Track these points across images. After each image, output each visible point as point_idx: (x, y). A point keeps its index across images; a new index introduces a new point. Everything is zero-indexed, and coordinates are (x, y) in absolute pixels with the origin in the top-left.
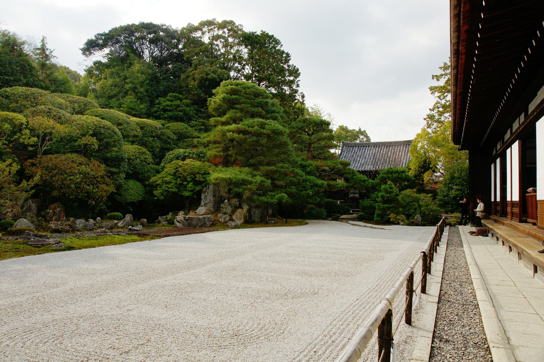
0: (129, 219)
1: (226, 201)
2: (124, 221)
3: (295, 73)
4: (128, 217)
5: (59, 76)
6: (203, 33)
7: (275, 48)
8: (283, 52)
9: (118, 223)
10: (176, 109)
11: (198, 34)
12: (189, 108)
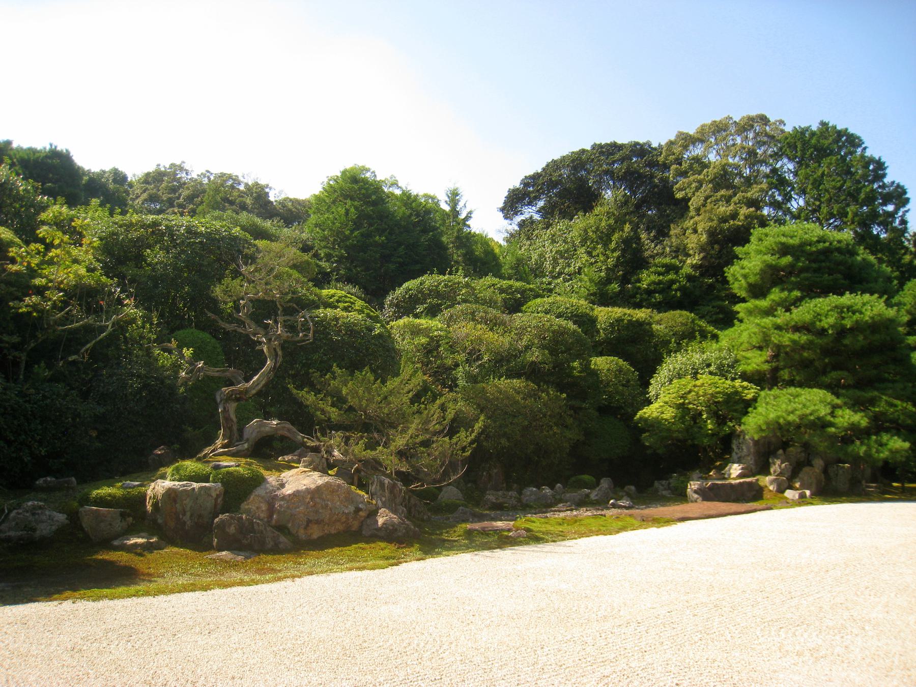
2: (223, 371)
3: (899, 196)
4: (605, 483)
5: (501, 258)
8: (871, 160)
11: (697, 151)
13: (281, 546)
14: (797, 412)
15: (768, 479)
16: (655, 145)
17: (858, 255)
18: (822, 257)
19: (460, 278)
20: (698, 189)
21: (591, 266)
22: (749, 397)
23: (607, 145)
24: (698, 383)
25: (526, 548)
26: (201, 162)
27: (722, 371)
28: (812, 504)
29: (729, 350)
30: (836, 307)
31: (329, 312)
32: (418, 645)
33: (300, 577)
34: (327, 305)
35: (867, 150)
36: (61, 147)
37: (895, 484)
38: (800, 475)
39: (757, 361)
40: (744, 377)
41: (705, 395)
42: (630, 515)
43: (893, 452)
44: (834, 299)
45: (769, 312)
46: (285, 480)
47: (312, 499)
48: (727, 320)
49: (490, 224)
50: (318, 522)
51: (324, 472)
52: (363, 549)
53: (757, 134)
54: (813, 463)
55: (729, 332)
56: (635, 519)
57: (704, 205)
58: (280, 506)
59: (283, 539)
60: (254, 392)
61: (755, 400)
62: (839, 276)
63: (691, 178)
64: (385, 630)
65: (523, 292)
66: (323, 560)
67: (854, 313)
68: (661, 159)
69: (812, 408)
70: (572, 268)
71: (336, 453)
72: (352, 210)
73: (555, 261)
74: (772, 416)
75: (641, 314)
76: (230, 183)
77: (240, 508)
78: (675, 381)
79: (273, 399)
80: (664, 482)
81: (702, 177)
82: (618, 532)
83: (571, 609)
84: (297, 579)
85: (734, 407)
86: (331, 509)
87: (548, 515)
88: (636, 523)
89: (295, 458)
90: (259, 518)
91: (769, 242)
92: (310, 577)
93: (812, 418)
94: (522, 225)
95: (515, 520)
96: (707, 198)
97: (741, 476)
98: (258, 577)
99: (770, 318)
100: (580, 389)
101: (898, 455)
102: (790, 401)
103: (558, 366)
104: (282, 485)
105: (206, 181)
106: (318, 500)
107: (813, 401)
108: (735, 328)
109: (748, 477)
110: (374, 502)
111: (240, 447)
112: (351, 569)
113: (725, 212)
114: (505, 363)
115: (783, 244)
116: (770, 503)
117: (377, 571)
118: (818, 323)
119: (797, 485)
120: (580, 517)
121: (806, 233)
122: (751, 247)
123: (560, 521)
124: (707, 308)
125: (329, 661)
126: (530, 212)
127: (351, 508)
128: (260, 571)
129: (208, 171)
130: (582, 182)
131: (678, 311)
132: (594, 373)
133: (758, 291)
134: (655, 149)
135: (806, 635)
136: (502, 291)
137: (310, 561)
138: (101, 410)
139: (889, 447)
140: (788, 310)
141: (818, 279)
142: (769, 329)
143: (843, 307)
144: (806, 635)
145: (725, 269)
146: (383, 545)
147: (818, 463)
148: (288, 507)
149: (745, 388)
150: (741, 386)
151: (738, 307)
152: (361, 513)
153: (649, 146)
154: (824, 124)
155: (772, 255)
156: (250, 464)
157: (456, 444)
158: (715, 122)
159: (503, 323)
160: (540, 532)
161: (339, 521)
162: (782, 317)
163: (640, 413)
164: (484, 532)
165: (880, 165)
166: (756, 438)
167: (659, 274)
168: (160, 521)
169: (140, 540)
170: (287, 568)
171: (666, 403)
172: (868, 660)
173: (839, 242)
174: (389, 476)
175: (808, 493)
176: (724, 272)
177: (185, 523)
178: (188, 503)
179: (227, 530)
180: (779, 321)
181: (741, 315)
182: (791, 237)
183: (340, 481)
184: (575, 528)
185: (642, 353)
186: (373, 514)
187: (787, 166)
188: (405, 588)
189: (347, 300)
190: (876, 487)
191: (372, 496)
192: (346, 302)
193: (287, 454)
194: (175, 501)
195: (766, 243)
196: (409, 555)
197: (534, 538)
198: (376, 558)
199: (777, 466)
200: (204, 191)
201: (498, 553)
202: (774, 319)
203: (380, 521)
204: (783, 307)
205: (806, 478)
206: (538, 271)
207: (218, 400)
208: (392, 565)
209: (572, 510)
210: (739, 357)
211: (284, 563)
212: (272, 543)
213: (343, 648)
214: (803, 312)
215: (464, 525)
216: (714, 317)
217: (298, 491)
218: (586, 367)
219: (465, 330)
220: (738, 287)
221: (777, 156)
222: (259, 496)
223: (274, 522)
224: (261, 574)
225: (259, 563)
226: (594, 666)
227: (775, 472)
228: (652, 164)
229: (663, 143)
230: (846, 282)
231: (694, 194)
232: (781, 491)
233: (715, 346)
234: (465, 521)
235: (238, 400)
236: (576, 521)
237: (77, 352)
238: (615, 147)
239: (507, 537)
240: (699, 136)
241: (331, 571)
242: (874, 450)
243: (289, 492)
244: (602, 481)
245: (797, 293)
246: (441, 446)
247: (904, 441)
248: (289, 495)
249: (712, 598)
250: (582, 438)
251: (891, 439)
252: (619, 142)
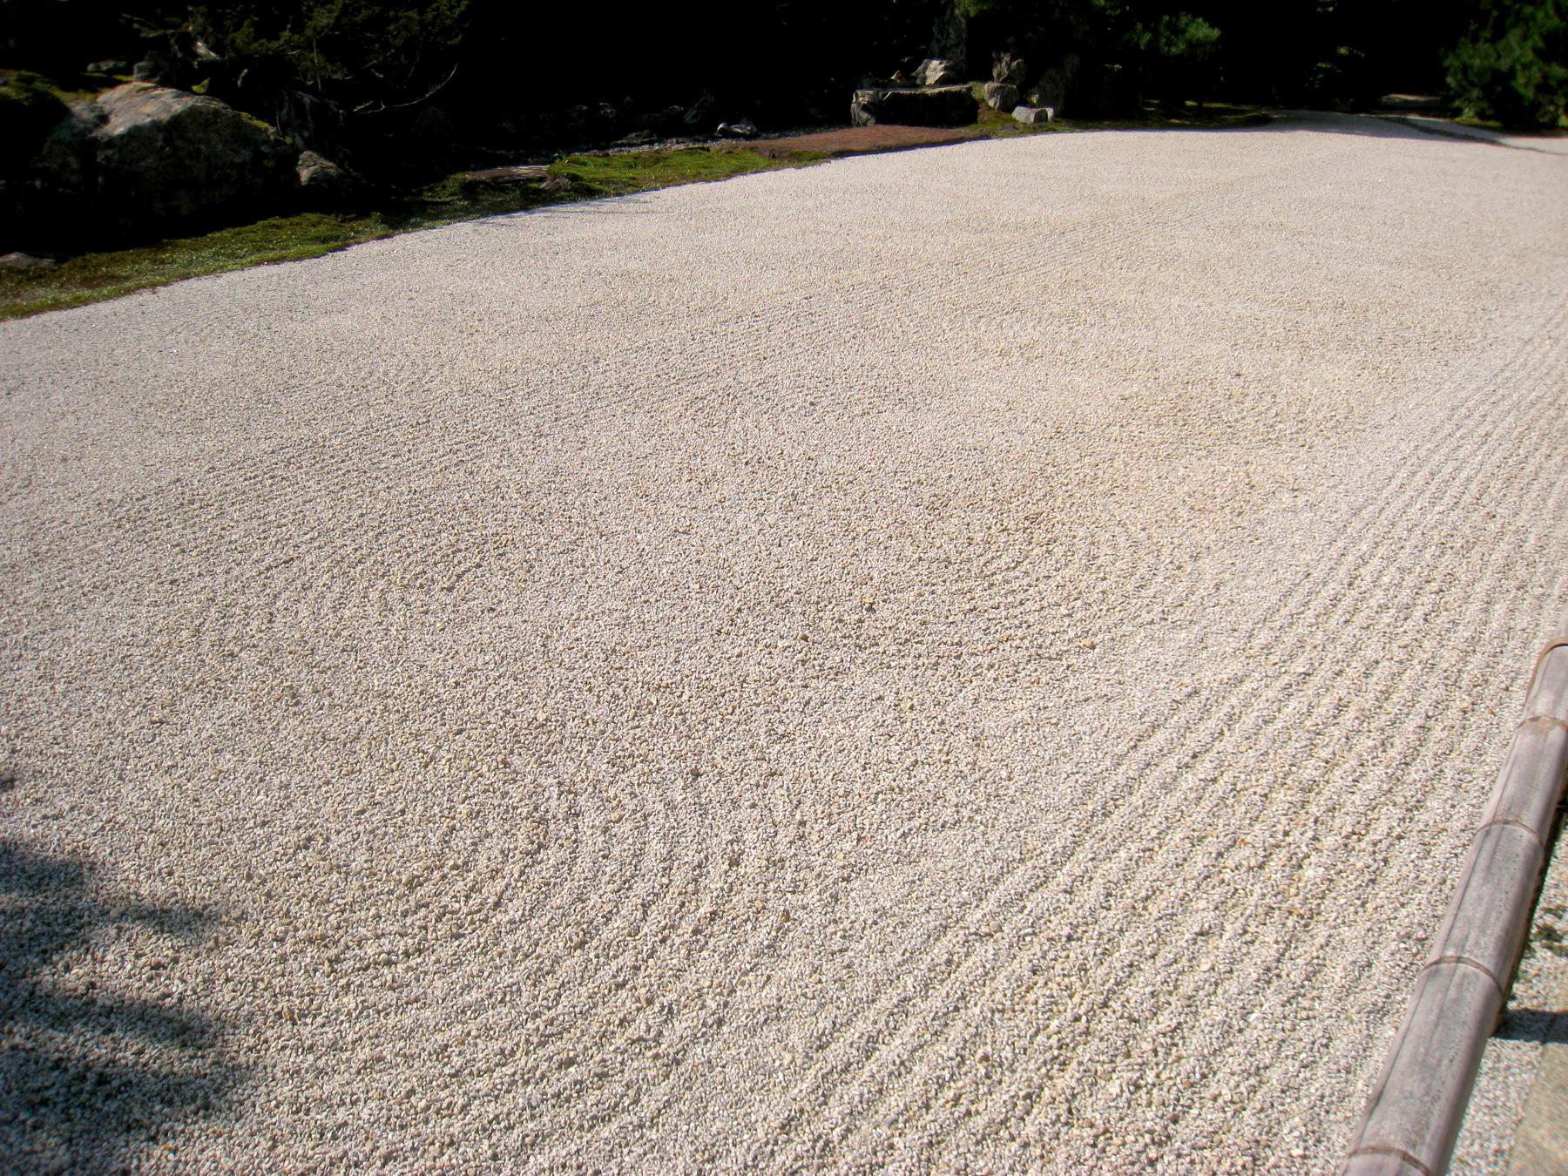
15: (987, 86)
25: (570, 208)
28: (1055, 131)
32: (386, 374)
33: (166, 284)
37: (1189, 103)
42: (752, 149)
43: (1193, 45)
46: (107, 108)
51: (184, 87)
52: (278, 227)
58: (107, 158)
64: (328, 355)
66: (206, 253)
71: (201, 48)
82: (729, 176)
83: (645, 300)
84: (162, 289)
87: (610, 152)
88: (762, 161)
89: (122, 64)
92: (185, 283)
95: (552, 162)
97: (942, 81)
98: (87, 293)
101: (1199, 51)
104: (104, 119)
106: (179, 143)
109: (955, 83)
110: (288, 140)
112: (258, 264)
116: (986, 129)
117: (306, 263)
119: (1034, 99)
120: (665, 154)
123: (631, 161)
125: (233, 413)
128: (88, 282)
135: (1017, 327)
137: (182, 257)
139: (1187, 35)
144: (1017, 327)
146: (313, 217)
156: (31, 80)
157: (433, 23)
160: (594, 180)
164: (497, 186)
170: (139, 272)
172: (1102, 360)
174: (311, 90)
175: (1050, 112)
183: (216, 104)
184: (658, 170)
186: (289, 161)
188: (358, 286)
190: (1157, 106)
191: (285, 128)
193: (105, 59)
196: (363, 232)
197: (584, 191)
198: (304, 240)
199: (1004, 65)
201: (521, 218)
203: (305, 175)
208: (334, 250)
209: (651, 143)
211: (129, 265)
213: (257, 391)
215: (460, 176)
222: (59, 142)
224: (91, 287)
225: (84, 267)
226: (682, 384)
227: (999, 75)
232: (1007, 108)
234: (465, 169)
236: (657, 161)
239: (537, 191)
241: (223, 269)
243: (120, 130)
246: (406, 27)
247: (1212, 26)
248: (122, 137)
249: (878, 276)
251: (1192, 21)
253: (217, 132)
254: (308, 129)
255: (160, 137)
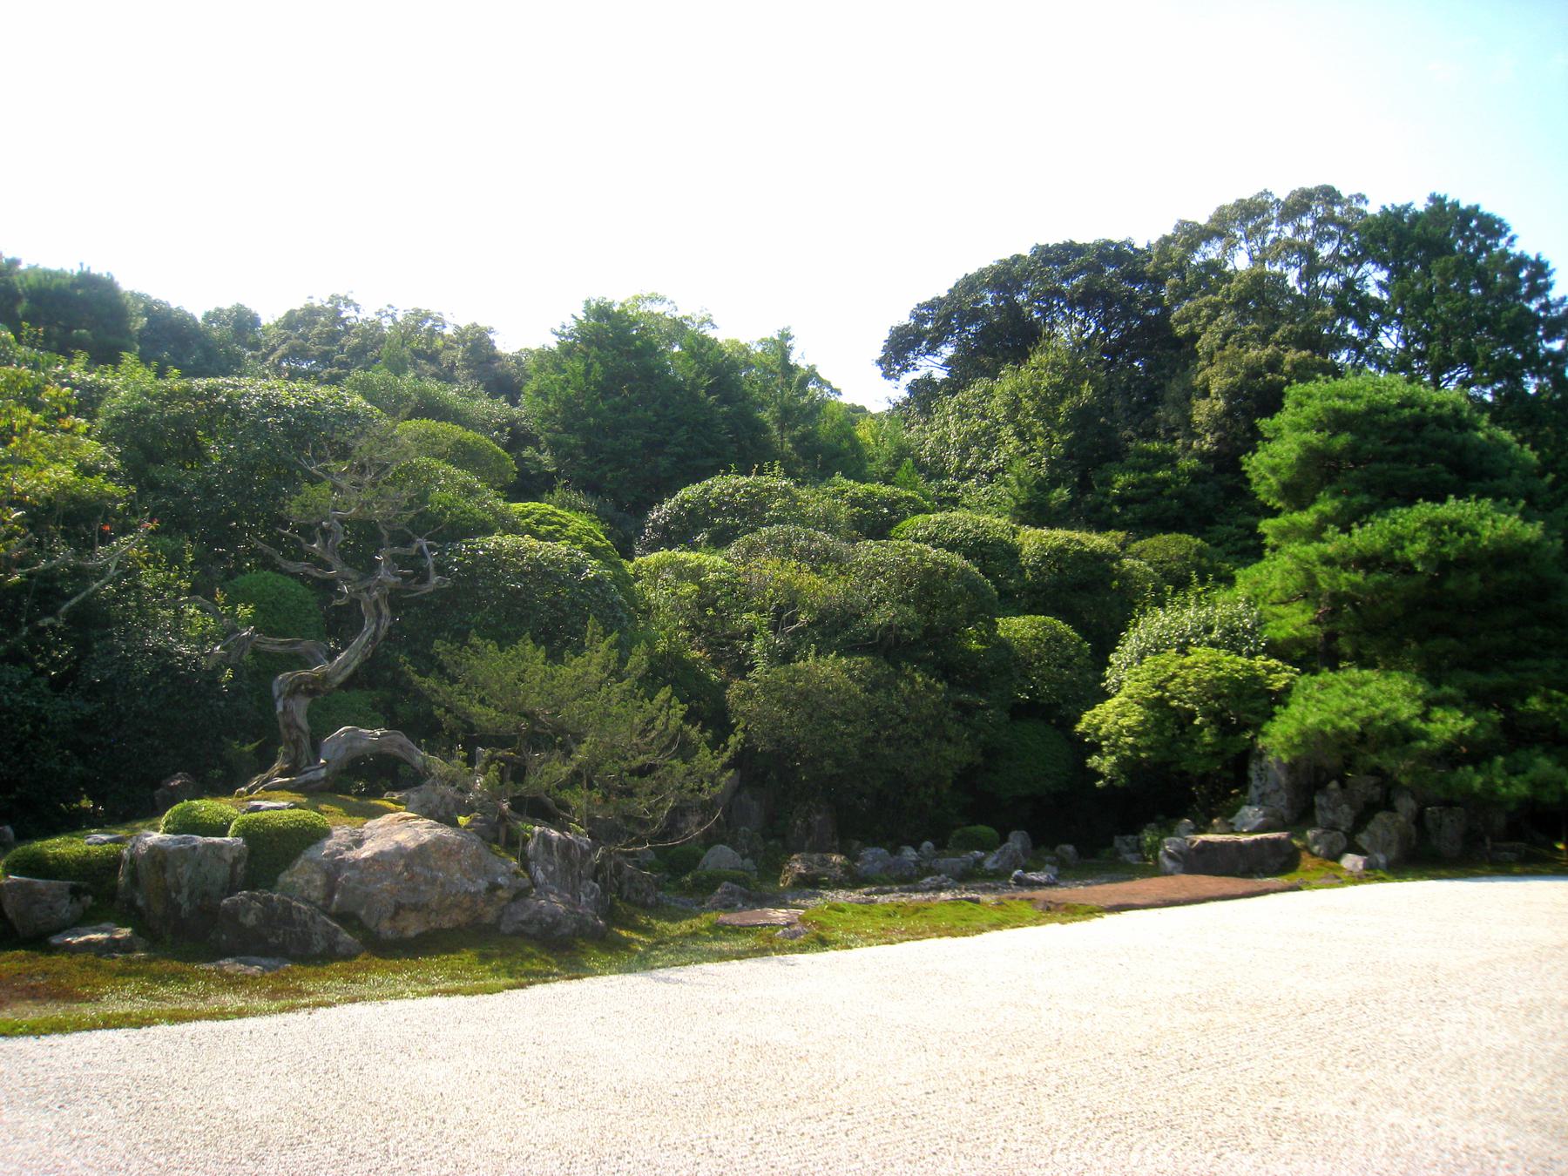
0: (1018, 846)
1: (1334, 785)
4: (1017, 841)
6: (1232, 245)
7: (1488, 249)
8: (1521, 261)
9: (983, 858)
10: (1159, 493)
11: (1211, 251)
12: (1200, 486)
13: (340, 949)
14: (1359, 714)
16: (1140, 244)
17: (1477, 429)
18: (1408, 434)
19: (777, 481)
20: (1210, 319)
21: (1021, 460)
22: (1279, 685)
23: (1058, 246)
24: (1188, 661)
26: (379, 295)
27: (1233, 640)
29: (1248, 600)
30: (1430, 523)
31: (509, 541)
34: (515, 529)
35: (1516, 242)
36: (98, 269)
38: (1370, 827)
39: (1295, 621)
40: (1273, 649)
41: (1198, 682)
44: (1424, 510)
45: (1315, 534)
46: (368, 833)
47: (406, 866)
48: (1253, 551)
49: (864, 387)
50: (416, 908)
53: (1319, 222)
54: (1396, 804)
55: (1252, 570)
56: (1034, 906)
57: (1221, 348)
59: (345, 936)
60: (340, 679)
61: (1287, 690)
62: (1440, 467)
63: (1201, 301)
65: (892, 504)
67: (1461, 534)
68: (1149, 267)
69: (1387, 705)
70: (993, 462)
72: (597, 365)
73: (964, 451)
74: (1311, 720)
75: (1099, 541)
76: (429, 323)
77: (275, 882)
78: (1149, 658)
79: (380, 690)
80: (1129, 838)
81: (1219, 298)
85: (1249, 703)
86: (443, 885)
90: (307, 901)
91: (1313, 408)
93: (1386, 724)
94: (914, 388)
96: (1226, 336)
99: (1315, 544)
100: (977, 676)
102: (1347, 693)
103: (931, 634)
105: (387, 323)
106: (417, 869)
107: (1381, 693)
108: (1264, 563)
111: (310, 776)
113: (1258, 358)
114: (836, 629)
115: (1337, 411)
118: (1397, 553)
121: (1380, 391)
122: (1282, 419)
124: (1227, 529)
126: (932, 366)
127: (482, 884)
129: (390, 306)
130: (1014, 310)
131: (1174, 535)
132: (1004, 645)
133: (1297, 494)
134: (1143, 251)
136: (854, 502)
138: (88, 709)
140: (1346, 529)
141: (1401, 473)
142: (1312, 564)
143: (1443, 523)
145: (1243, 458)
147: (1406, 805)
148: (361, 882)
149: (1270, 670)
150: (1264, 667)
151: (1266, 526)
152: (500, 893)
153: (1131, 246)
154: (1437, 201)
155: (1319, 431)
158: (1242, 201)
159: (838, 559)
161: (458, 905)
162: (1335, 542)
163: (1086, 717)
165: (1540, 269)
166: (1285, 759)
167: (1142, 469)
168: (140, 903)
169: (99, 936)
171: (1131, 697)
173: (1440, 405)
176: (1241, 464)
177: (180, 906)
178: (186, 872)
179: (242, 919)
180: (1330, 549)
181: (1270, 540)
182: (1353, 398)
185: (1095, 605)
187: (1373, 279)
189: (555, 519)
192: (552, 523)
194: (164, 869)
195: (1307, 410)
200: (382, 339)
202: (1322, 546)
204: (1337, 525)
205: (1379, 833)
206: (934, 472)
207: (276, 693)
210: (1266, 615)
212: (323, 944)
214: (1368, 536)
216: (1240, 544)
217: (382, 853)
218: (990, 638)
219: (772, 571)
220: (1265, 486)
221: (1356, 260)
222: (311, 860)
223: (333, 907)
228: (1135, 277)
229: (1153, 242)
230: (1454, 478)
231: (1204, 329)
233: (1227, 596)
235: (311, 693)
237: (53, 613)
238: (1069, 251)
240: (1214, 226)
242: (1500, 782)
244: (1012, 835)
245: (1365, 499)
248: (366, 860)
250: (980, 760)
252: (1079, 241)
253: (459, 861)
254: (553, 864)
255: (402, 862)
